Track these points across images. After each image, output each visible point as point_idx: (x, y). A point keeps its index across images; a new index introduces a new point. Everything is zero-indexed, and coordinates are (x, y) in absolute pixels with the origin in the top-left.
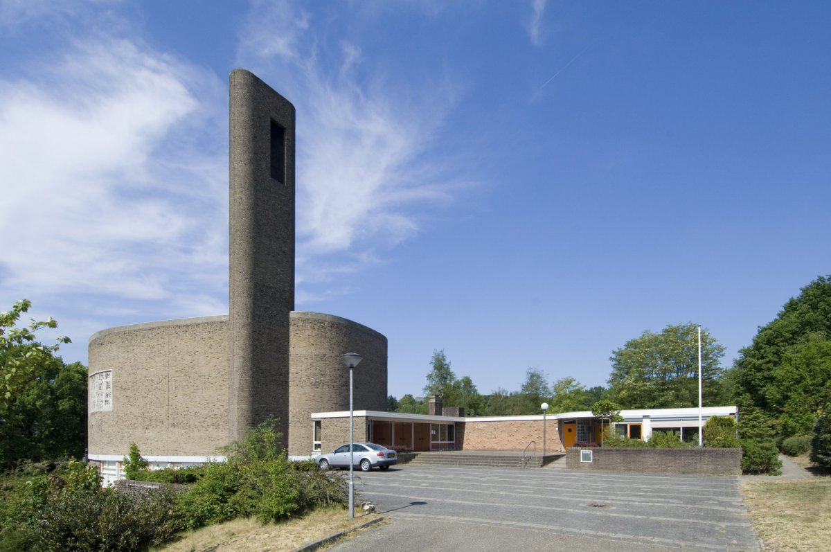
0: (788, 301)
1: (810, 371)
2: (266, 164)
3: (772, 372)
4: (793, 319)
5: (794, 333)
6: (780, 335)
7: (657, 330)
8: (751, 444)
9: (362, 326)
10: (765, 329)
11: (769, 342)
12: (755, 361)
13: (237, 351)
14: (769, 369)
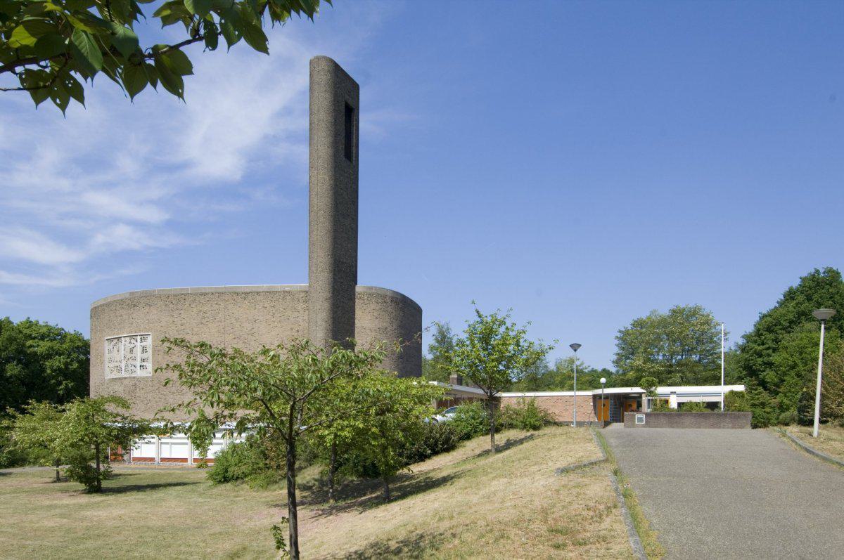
0: (787, 289)
1: (802, 359)
2: (342, 147)
3: (771, 358)
4: (791, 309)
5: (791, 322)
6: (778, 323)
7: (664, 311)
8: (758, 411)
9: (415, 303)
10: (765, 316)
11: (769, 330)
12: (756, 347)
13: (320, 323)
14: (769, 355)
